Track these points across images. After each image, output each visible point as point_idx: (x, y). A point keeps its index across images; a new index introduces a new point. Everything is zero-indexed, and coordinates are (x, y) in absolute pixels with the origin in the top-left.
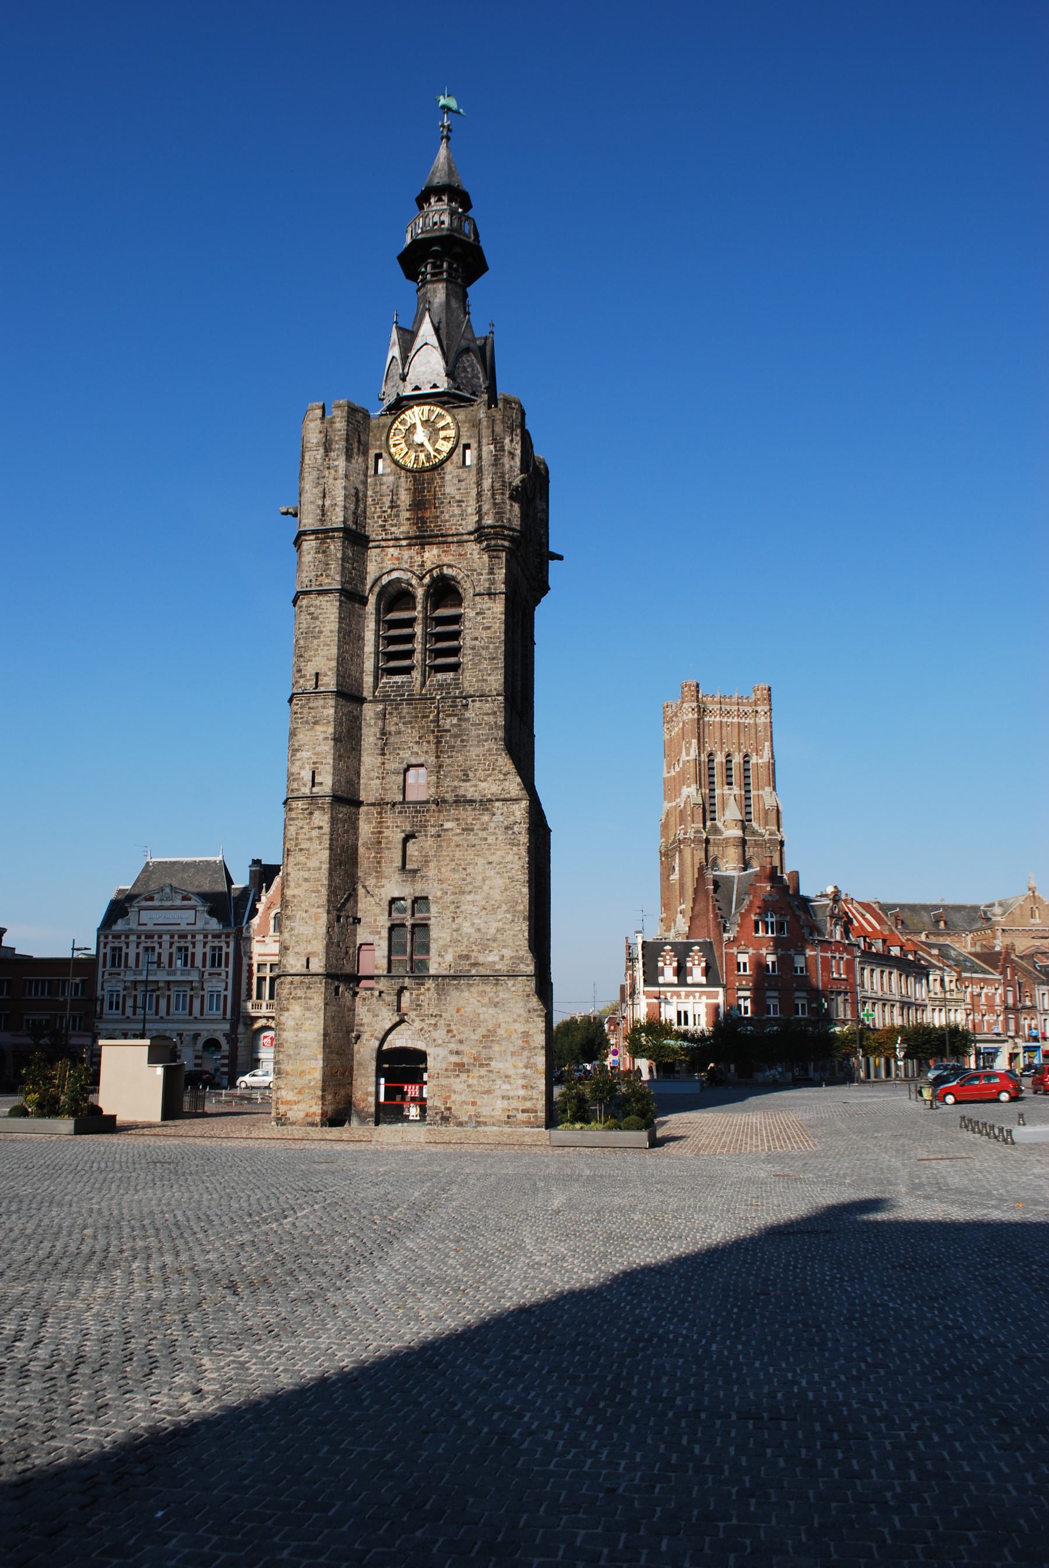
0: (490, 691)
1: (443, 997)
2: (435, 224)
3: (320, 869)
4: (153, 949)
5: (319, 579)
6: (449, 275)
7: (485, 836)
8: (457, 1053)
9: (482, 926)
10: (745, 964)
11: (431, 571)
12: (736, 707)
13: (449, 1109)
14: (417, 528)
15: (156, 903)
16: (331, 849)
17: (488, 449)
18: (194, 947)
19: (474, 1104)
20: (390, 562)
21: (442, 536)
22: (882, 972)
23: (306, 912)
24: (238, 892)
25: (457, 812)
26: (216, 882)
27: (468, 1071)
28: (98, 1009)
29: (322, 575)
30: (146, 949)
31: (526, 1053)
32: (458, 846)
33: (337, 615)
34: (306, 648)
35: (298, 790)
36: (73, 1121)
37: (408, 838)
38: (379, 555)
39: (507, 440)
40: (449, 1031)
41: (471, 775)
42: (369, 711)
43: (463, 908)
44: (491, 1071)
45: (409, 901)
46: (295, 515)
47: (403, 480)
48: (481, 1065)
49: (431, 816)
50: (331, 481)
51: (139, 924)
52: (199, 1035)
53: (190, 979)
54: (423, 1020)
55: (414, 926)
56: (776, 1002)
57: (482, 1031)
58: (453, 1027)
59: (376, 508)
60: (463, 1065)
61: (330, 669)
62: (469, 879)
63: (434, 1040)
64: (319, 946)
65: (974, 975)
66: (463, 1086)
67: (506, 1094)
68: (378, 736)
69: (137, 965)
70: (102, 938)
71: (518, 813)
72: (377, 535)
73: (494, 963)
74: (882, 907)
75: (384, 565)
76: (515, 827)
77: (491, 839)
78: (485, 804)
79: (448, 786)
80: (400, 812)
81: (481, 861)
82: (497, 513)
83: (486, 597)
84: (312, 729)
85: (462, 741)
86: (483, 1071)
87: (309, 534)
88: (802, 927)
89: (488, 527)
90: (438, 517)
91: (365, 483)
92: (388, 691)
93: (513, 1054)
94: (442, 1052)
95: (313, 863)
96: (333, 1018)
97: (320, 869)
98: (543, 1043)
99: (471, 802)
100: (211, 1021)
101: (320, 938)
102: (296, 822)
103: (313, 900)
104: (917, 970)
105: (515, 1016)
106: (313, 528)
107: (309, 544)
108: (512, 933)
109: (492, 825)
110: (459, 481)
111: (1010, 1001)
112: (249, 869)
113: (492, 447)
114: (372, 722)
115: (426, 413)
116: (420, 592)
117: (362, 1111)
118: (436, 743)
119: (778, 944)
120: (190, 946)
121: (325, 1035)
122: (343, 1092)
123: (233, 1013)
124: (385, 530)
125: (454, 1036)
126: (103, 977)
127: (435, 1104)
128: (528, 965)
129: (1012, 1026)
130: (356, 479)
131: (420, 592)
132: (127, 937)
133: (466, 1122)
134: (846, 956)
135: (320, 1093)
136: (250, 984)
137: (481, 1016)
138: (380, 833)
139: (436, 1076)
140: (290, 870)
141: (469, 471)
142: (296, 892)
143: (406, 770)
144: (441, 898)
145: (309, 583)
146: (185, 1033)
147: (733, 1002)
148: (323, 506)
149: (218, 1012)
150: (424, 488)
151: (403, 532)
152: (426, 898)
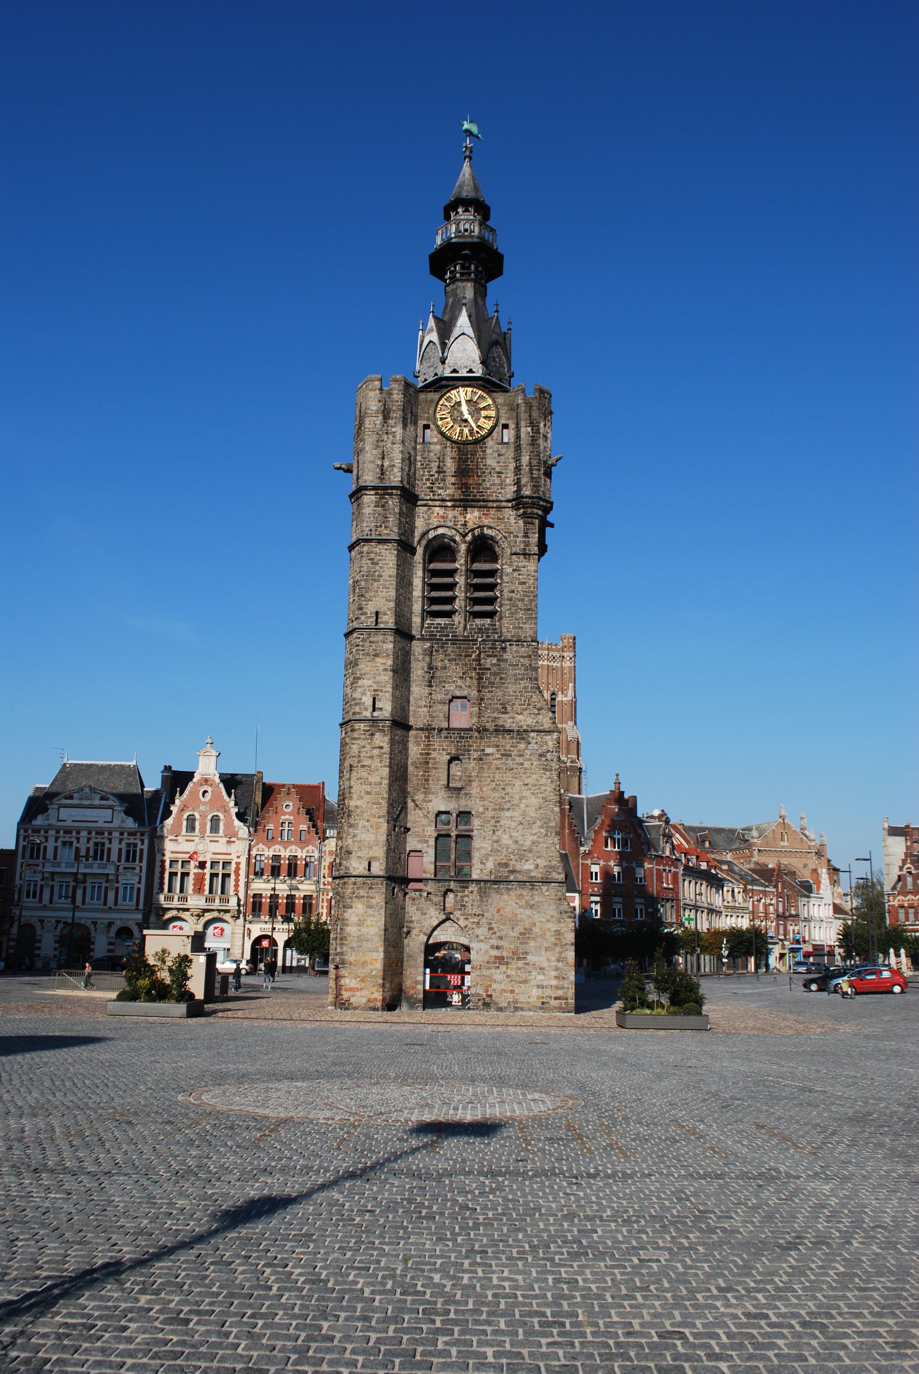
0: (526, 637)
2: (466, 230)
3: (381, 783)
4: (71, 843)
5: (379, 529)
6: (476, 276)
7: (521, 761)
8: (498, 948)
9: (519, 838)
10: (596, 873)
11: (472, 530)
12: (546, 652)
13: (490, 996)
15: (75, 802)
16: (390, 767)
17: (526, 431)
18: (110, 843)
19: (512, 992)
21: (484, 501)
22: (696, 883)
23: (368, 821)
24: (150, 794)
26: (131, 785)
27: (507, 963)
28: (16, 897)
30: (64, 843)
31: (558, 949)
32: (498, 769)
34: (367, 589)
35: (359, 713)
36: (185, 1005)
37: (454, 759)
39: (542, 425)
40: (490, 929)
41: (509, 708)
42: (417, 648)
43: (502, 822)
44: (528, 964)
45: (454, 815)
46: (349, 471)
47: (448, 449)
48: (519, 959)
50: (389, 445)
51: (59, 820)
52: (113, 923)
53: (106, 872)
54: (467, 919)
55: (458, 836)
56: (620, 906)
57: (519, 929)
58: (494, 925)
60: (503, 958)
61: (389, 609)
62: (507, 798)
64: (380, 852)
65: (755, 888)
66: (503, 977)
67: (540, 983)
69: (55, 858)
70: (22, 832)
71: (550, 743)
73: (530, 871)
74: (685, 828)
75: (431, 521)
77: (527, 764)
78: (522, 734)
80: (446, 737)
81: (518, 783)
82: (534, 486)
83: (522, 557)
84: (372, 660)
85: (501, 678)
86: (520, 964)
88: (642, 844)
89: (527, 497)
90: (480, 484)
91: (415, 449)
93: (547, 949)
94: (484, 946)
95: (375, 778)
96: (391, 915)
97: (381, 783)
98: (573, 940)
99: (510, 731)
100: (125, 911)
101: (381, 844)
103: (374, 811)
104: (717, 883)
105: (549, 917)
106: (372, 484)
107: (369, 499)
108: (545, 845)
109: (528, 752)
110: (499, 455)
111: (781, 910)
112: (160, 774)
113: (529, 429)
114: (421, 657)
115: (469, 393)
117: (412, 997)
119: (623, 858)
120: (107, 842)
121: (386, 930)
122: (396, 981)
123: (145, 904)
125: (495, 933)
126: (21, 867)
128: (559, 873)
129: (781, 932)
130: (409, 445)
131: (463, 547)
132: (46, 832)
133: (506, 1008)
134: (673, 869)
135: (381, 981)
136: (162, 878)
137: (519, 916)
138: (428, 754)
140: (352, 783)
141: (508, 448)
142: (359, 803)
143: (451, 701)
144: (483, 813)
146: (99, 922)
147: (586, 905)
148: (382, 466)
149: (131, 903)
151: (449, 495)
152: (469, 813)
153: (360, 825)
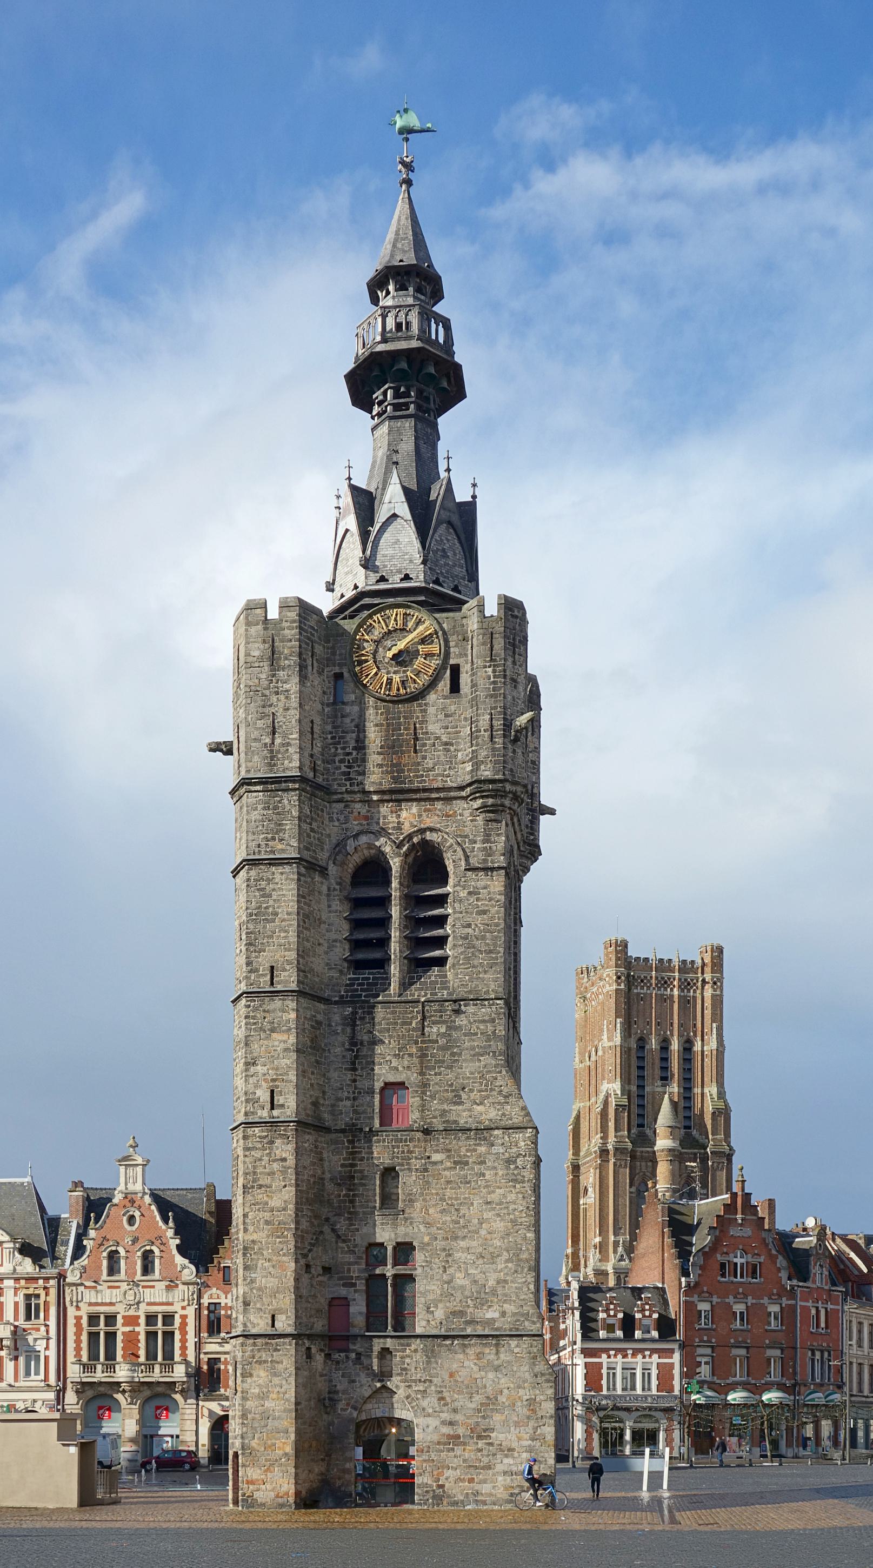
0: (487, 992)
1: (433, 1360)
3: (284, 1209)
6: (419, 407)
8: (451, 1423)
11: (410, 837)
13: (442, 1486)
14: (393, 778)
16: (297, 1185)
20: (356, 823)
21: (425, 790)
25: (447, 1141)
29: (273, 839)
31: (532, 1423)
32: (448, 1182)
33: (295, 892)
38: (342, 812)
41: (464, 1096)
43: (457, 1255)
44: (491, 1444)
49: (415, 1147)
53: (142, 1337)
54: (409, 1387)
58: (446, 1394)
59: (337, 749)
60: (458, 1437)
63: (424, 1409)
64: (287, 1301)
68: (347, 1045)
72: (339, 785)
73: (494, 1320)
76: (518, 1160)
77: (489, 1175)
78: (482, 1132)
79: (435, 1110)
84: (267, 1038)
87: (255, 784)
88: (779, 1270)
90: (419, 764)
92: (357, 990)
93: (517, 1424)
94: (433, 1422)
96: (305, 1386)
98: (552, 1411)
102: (253, 1153)
110: (446, 716)
114: (339, 1029)
116: (395, 864)
118: (420, 1057)
120: (43, 1293)
124: (350, 779)
127: (425, 1481)
128: (534, 1323)
138: (352, 1165)
139: (425, 1449)
144: (428, 1244)
145: (257, 850)
150: (400, 724)
153: (259, 1265)
